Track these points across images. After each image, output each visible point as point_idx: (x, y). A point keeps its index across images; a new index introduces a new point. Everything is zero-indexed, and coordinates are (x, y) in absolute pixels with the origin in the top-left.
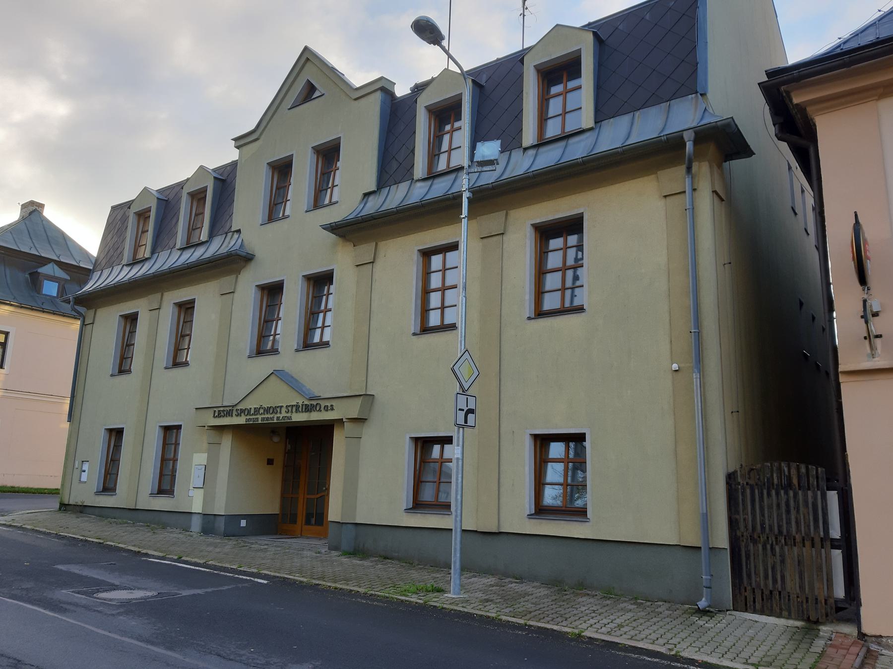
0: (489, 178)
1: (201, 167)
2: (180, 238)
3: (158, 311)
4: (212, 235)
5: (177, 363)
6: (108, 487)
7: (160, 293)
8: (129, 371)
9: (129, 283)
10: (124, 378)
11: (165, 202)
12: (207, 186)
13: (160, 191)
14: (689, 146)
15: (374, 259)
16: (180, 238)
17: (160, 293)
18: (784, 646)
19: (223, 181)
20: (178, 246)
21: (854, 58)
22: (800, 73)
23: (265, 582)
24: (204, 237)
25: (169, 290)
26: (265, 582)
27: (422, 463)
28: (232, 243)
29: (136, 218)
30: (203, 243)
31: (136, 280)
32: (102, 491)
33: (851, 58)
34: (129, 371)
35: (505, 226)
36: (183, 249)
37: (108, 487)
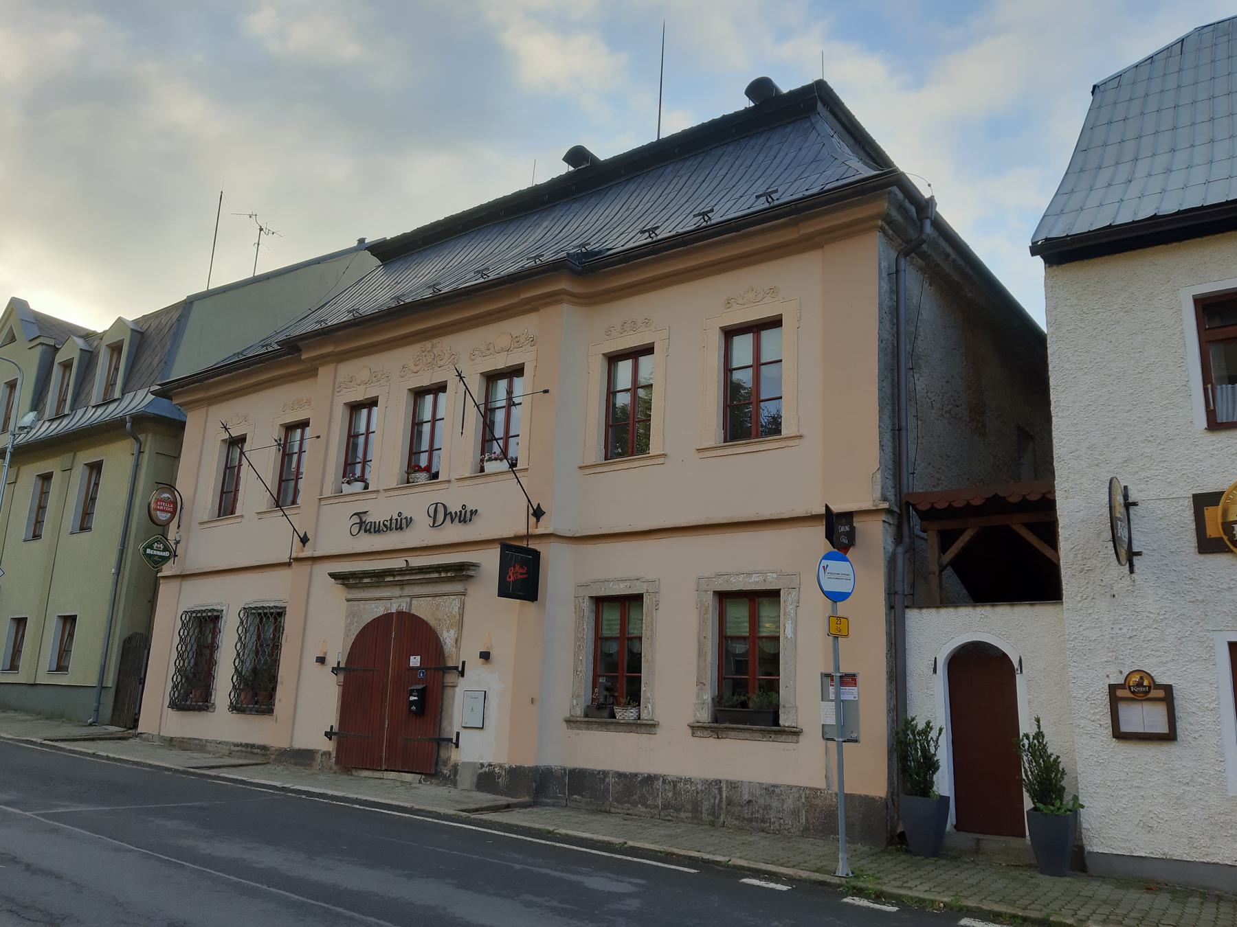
0: (22, 439)
1: (120, 319)
2: (96, 394)
3: (69, 472)
4: (73, 408)
5: (84, 527)
6: (61, 667)
7: (73, 454)
8: (89, 529)
9: (58, 437)
10: (85, 536)
11: (88, 354)
12: (123, 339)
13: (136, 322)
14: (128, 425)
15: (16, 479)
16: (96, 394)
17: (73, 454)
18: (1164, 910)
19: (142, 333)
20: (93, 403)
21: (660, 246)
22: (798, 206)
23: (785, 888)
24: (117, 395)
25: (26, 463)
26: (785, 888)
27: (599, 641)
28: (43, 429)
29: (109, 351)
30: (115, 400)
31: (83, 430)
32: (56, 671)
33: (737, 223)
34: (89, 529)
35: (72, 464)
36: (97, 406)
37: (61, 667)
